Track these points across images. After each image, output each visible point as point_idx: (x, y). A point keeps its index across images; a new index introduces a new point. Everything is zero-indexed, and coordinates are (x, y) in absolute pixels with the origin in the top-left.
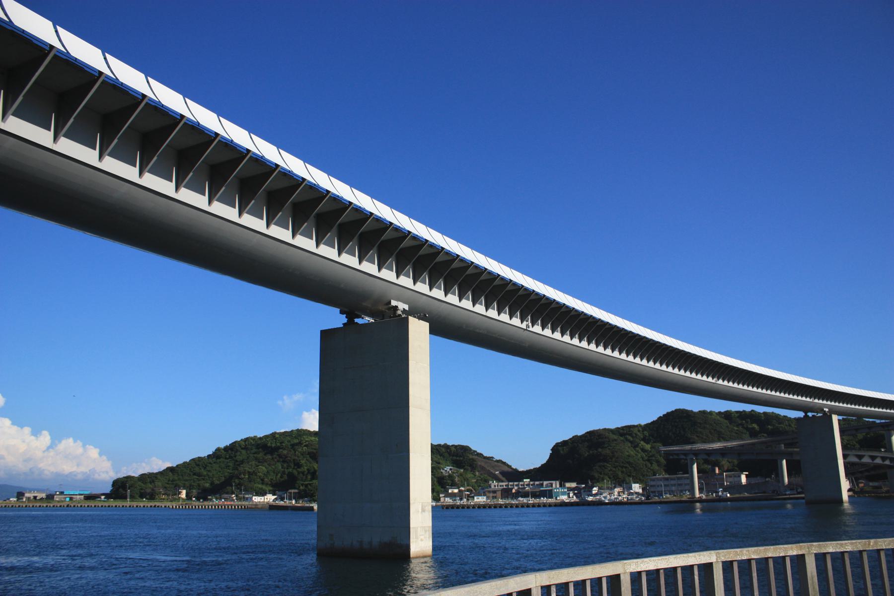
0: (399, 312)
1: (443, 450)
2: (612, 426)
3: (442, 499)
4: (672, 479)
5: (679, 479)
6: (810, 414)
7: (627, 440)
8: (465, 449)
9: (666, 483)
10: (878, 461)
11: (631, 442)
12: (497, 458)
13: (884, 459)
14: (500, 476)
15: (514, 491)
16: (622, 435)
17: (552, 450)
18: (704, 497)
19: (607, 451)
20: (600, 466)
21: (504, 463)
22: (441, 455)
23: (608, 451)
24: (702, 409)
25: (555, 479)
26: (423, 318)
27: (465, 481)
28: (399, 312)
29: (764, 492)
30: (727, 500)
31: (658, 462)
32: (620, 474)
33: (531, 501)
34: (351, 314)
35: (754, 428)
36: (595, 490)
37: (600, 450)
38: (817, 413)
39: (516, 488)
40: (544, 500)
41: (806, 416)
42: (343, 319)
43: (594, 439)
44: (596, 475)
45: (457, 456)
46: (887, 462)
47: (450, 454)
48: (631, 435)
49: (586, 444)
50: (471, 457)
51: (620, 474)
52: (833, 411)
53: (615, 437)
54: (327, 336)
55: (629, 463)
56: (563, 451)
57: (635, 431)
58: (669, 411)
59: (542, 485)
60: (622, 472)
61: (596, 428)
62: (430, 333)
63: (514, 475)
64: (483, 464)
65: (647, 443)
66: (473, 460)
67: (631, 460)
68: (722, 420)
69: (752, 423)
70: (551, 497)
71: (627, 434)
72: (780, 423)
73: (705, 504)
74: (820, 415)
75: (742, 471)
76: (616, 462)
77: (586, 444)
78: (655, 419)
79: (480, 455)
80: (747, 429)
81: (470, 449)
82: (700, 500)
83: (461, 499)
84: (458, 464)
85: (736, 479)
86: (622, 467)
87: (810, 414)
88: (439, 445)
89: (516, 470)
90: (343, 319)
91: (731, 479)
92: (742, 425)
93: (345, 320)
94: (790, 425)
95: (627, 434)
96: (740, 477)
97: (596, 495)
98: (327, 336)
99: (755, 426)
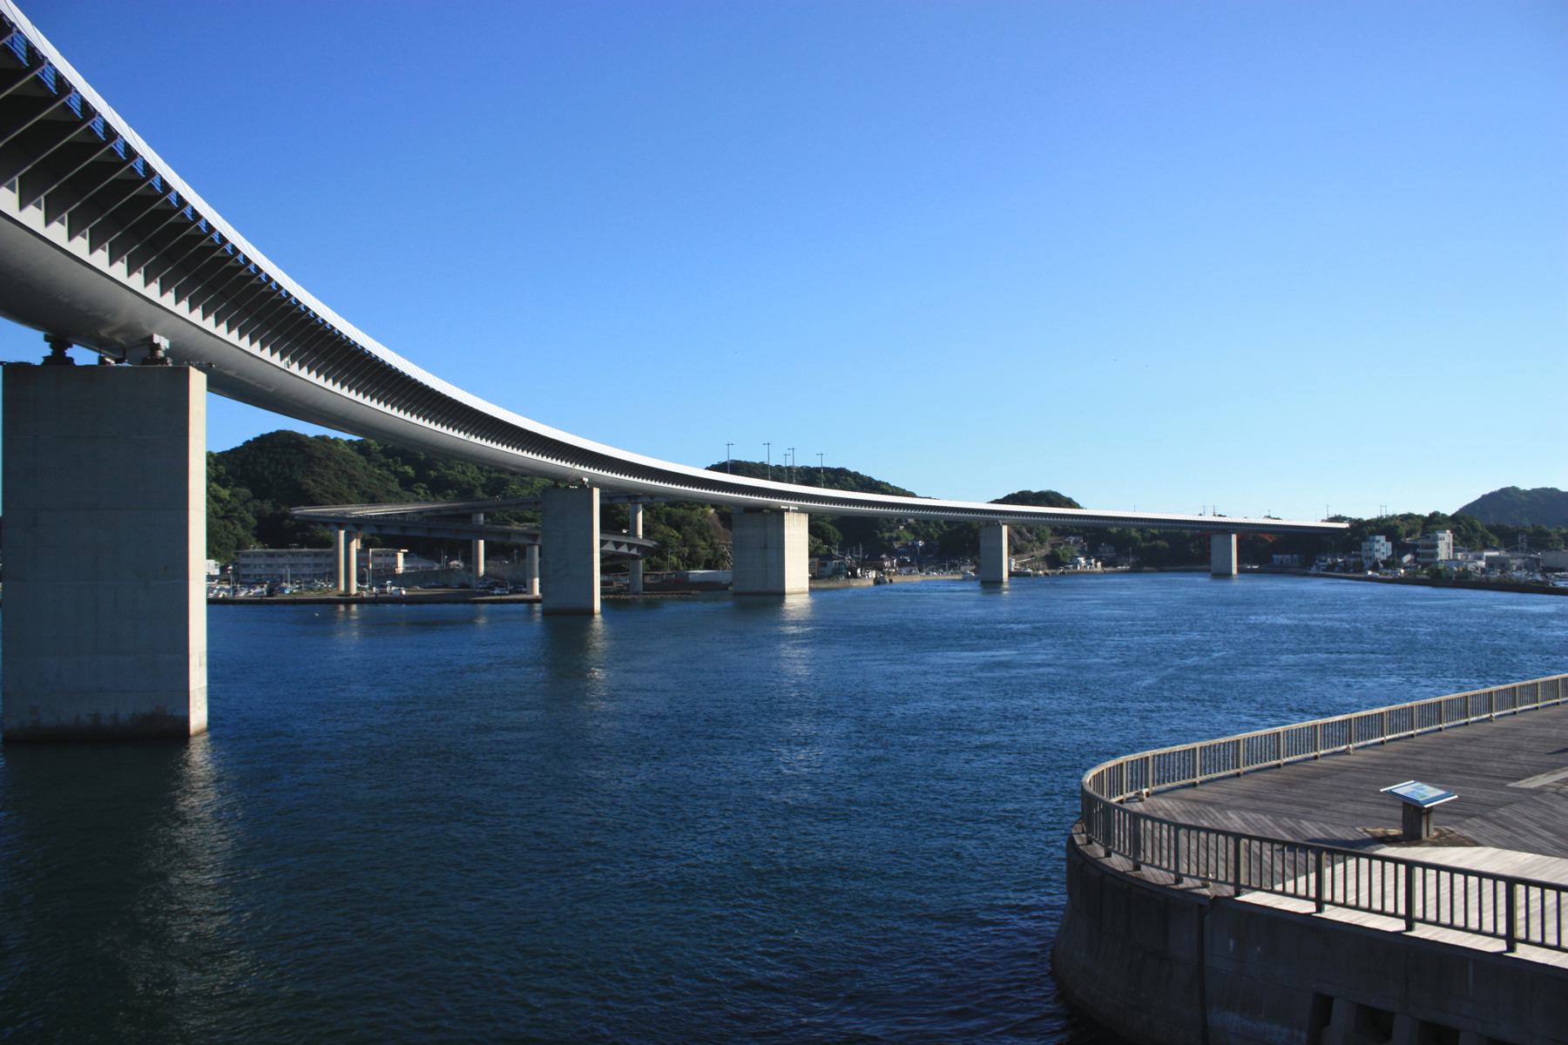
0: (161, 354)
4: (280, 556)
5: (293, 554)
9: (270, 561)
10: (624, 549)
13: (630, 546)
18: (365, 594)
26: (200, 368)
28: (161, 354)
29: (446, 586)
30: (399, 600)
31: (242, 520)
34: (59, 343)
42: (47, 350)
46: (634, 552)
52: (594, 483)
58: (266, 432)
62: (209, 390)
65: (224, 487)
68: (355, 454)
69: (404, 464)
73: (366, 607)
75: (399, 548)
78: (239, 444)
80: (396, 473)
82: (360, 601)
85: (388, 560)
86: (1114, 712)
90: (47, 350)
91: (379, 560)
92: (388, 466)
93: (48, 351)
96: (395, 556)
99: (408, 469)
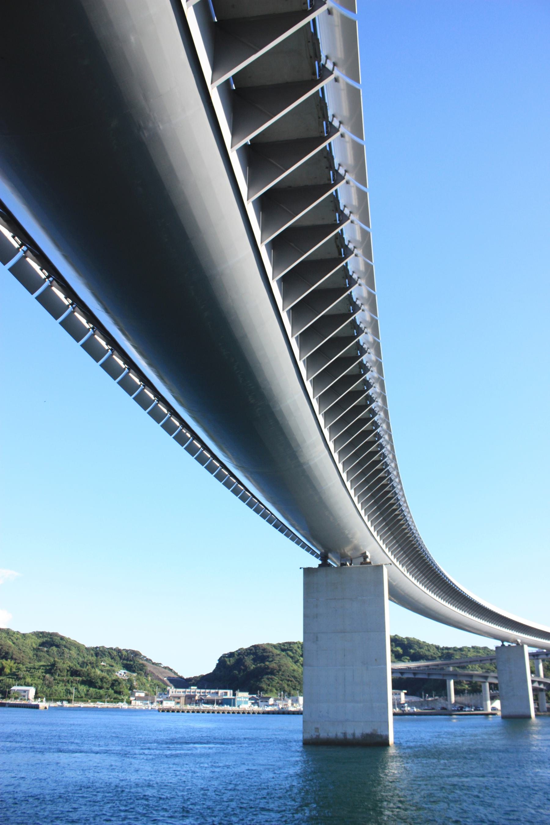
1: (115, 653)
2: (275, 642)
3: (133, 702)
6: (506, 644)
7: (288, 655)
8: (136, 654)
11: (292, 658)
12: (164, 664)
14: (168, 682)
15: (197, 698)
16: (283, 650)
17: (219, 660)
19: (273, 665)
20: (268, 679)
21: (171, 670)
22: (112, 658)
23: (275, 665)
24: (411, 635)
25: (229, 689)
27: (142, 687)
29: (433, 709)
32: (286, 686)
33: (216, 707)
35: (398, 651)
36: (271, 701)
37: (267, 663)
38: (512, 643)
39: (198, 695)
40: (227, 707)
41: (503, 645)
43: (258, 653)
44: (264, 686)
45: (127, 660)
46: (542, 686)
47: (121, 658)
48: (291, 650)
49: (252, 657)
50: (141, 662)
51: (286, 686)
53: (278, 652)
54: (308, 571)
55: (294, 677)
56: (230, 662)
57: (295, 647)
59: (217, 693)
60: (288, 685)
61: (62, 633)
63: (181, 683)
64: (152, 670)
66: (144, 665)
67: (296, 674)
70: (234, 705)
71: (288, 650)
72: (420, 648)
74: (514, 645)
75: (402, 689)
76: (282, 675)
77: (252, 657)
79: (148, 660)
81: (141, 655)
83: (152, 703)
84: (128, 668)
86: (288, 680)
87: (506, 644)
88: (112, 649)
89: (181, 678)
93: (320, 562)
94: (429, 650)
95: (288, 650)
97: (273, 705)
98: (308, 571)
